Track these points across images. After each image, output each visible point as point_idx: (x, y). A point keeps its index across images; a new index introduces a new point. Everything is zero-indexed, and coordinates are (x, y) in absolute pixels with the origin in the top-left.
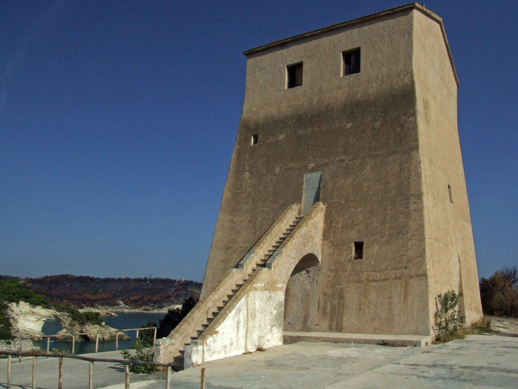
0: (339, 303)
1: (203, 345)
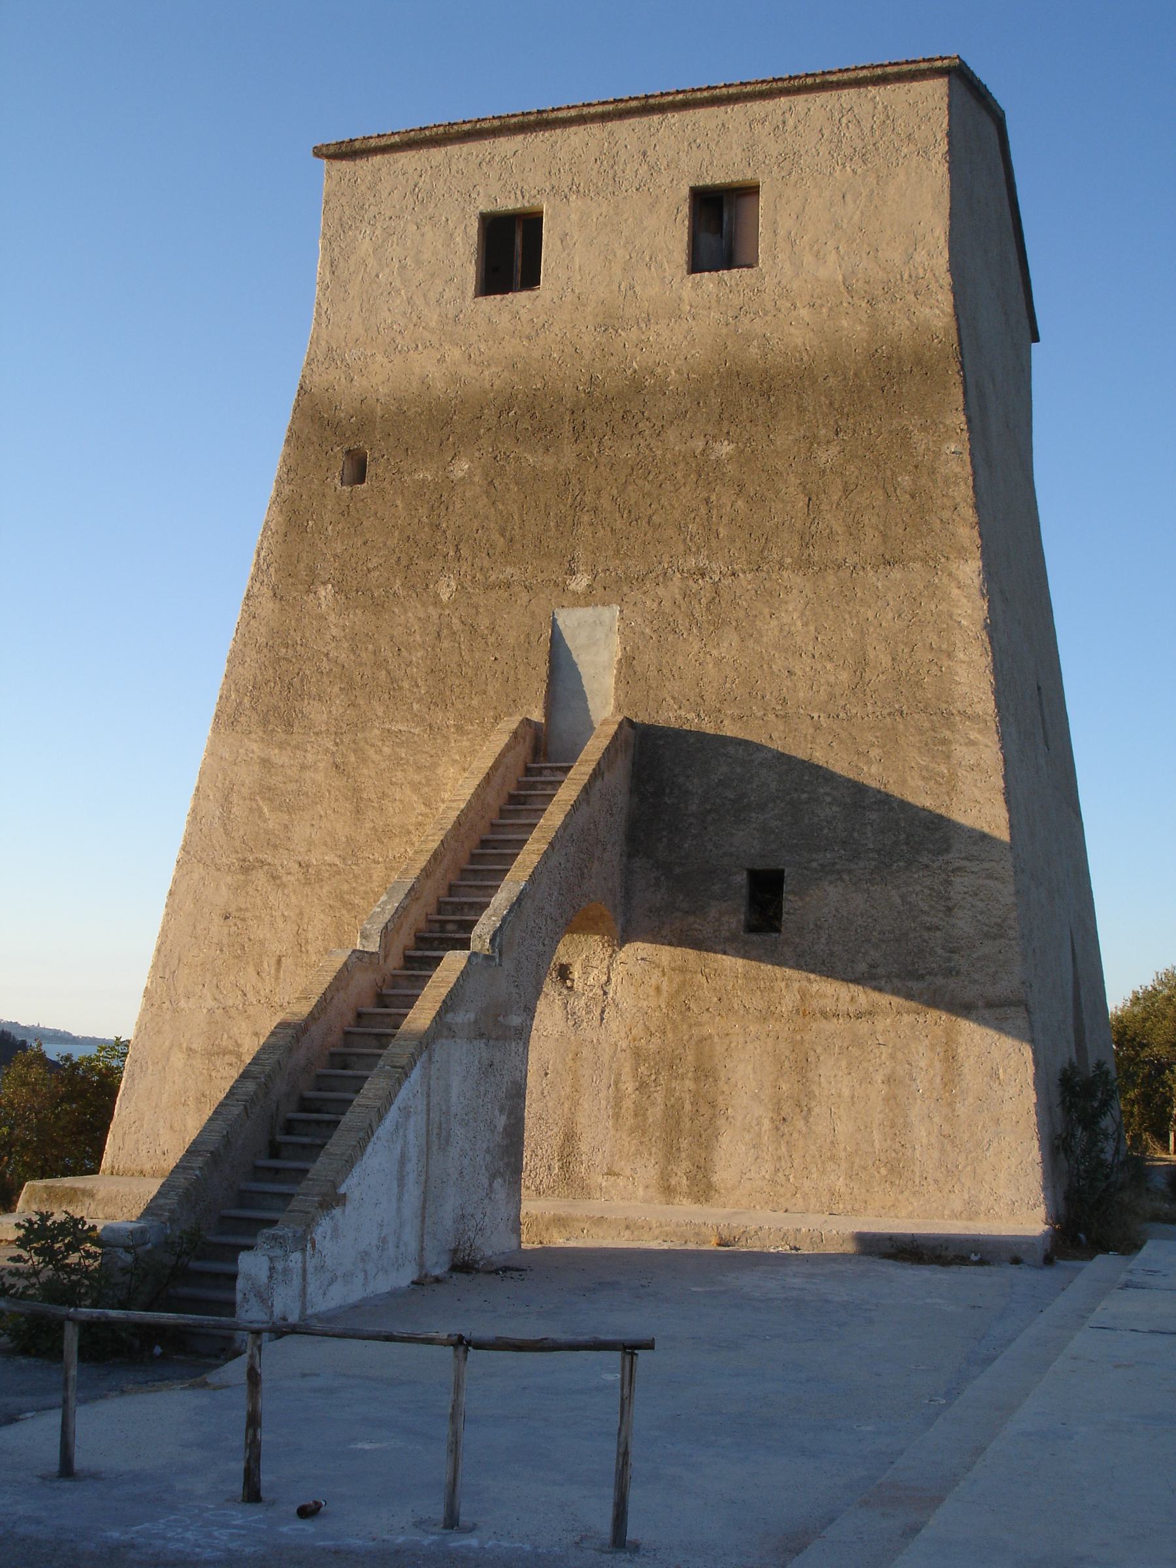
0: (696, 1096)
1: (304, 1250)
